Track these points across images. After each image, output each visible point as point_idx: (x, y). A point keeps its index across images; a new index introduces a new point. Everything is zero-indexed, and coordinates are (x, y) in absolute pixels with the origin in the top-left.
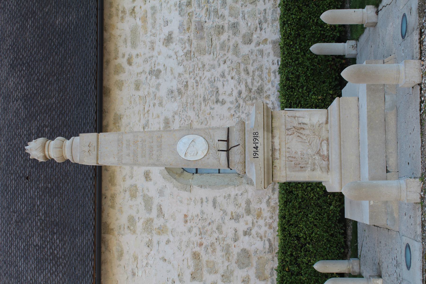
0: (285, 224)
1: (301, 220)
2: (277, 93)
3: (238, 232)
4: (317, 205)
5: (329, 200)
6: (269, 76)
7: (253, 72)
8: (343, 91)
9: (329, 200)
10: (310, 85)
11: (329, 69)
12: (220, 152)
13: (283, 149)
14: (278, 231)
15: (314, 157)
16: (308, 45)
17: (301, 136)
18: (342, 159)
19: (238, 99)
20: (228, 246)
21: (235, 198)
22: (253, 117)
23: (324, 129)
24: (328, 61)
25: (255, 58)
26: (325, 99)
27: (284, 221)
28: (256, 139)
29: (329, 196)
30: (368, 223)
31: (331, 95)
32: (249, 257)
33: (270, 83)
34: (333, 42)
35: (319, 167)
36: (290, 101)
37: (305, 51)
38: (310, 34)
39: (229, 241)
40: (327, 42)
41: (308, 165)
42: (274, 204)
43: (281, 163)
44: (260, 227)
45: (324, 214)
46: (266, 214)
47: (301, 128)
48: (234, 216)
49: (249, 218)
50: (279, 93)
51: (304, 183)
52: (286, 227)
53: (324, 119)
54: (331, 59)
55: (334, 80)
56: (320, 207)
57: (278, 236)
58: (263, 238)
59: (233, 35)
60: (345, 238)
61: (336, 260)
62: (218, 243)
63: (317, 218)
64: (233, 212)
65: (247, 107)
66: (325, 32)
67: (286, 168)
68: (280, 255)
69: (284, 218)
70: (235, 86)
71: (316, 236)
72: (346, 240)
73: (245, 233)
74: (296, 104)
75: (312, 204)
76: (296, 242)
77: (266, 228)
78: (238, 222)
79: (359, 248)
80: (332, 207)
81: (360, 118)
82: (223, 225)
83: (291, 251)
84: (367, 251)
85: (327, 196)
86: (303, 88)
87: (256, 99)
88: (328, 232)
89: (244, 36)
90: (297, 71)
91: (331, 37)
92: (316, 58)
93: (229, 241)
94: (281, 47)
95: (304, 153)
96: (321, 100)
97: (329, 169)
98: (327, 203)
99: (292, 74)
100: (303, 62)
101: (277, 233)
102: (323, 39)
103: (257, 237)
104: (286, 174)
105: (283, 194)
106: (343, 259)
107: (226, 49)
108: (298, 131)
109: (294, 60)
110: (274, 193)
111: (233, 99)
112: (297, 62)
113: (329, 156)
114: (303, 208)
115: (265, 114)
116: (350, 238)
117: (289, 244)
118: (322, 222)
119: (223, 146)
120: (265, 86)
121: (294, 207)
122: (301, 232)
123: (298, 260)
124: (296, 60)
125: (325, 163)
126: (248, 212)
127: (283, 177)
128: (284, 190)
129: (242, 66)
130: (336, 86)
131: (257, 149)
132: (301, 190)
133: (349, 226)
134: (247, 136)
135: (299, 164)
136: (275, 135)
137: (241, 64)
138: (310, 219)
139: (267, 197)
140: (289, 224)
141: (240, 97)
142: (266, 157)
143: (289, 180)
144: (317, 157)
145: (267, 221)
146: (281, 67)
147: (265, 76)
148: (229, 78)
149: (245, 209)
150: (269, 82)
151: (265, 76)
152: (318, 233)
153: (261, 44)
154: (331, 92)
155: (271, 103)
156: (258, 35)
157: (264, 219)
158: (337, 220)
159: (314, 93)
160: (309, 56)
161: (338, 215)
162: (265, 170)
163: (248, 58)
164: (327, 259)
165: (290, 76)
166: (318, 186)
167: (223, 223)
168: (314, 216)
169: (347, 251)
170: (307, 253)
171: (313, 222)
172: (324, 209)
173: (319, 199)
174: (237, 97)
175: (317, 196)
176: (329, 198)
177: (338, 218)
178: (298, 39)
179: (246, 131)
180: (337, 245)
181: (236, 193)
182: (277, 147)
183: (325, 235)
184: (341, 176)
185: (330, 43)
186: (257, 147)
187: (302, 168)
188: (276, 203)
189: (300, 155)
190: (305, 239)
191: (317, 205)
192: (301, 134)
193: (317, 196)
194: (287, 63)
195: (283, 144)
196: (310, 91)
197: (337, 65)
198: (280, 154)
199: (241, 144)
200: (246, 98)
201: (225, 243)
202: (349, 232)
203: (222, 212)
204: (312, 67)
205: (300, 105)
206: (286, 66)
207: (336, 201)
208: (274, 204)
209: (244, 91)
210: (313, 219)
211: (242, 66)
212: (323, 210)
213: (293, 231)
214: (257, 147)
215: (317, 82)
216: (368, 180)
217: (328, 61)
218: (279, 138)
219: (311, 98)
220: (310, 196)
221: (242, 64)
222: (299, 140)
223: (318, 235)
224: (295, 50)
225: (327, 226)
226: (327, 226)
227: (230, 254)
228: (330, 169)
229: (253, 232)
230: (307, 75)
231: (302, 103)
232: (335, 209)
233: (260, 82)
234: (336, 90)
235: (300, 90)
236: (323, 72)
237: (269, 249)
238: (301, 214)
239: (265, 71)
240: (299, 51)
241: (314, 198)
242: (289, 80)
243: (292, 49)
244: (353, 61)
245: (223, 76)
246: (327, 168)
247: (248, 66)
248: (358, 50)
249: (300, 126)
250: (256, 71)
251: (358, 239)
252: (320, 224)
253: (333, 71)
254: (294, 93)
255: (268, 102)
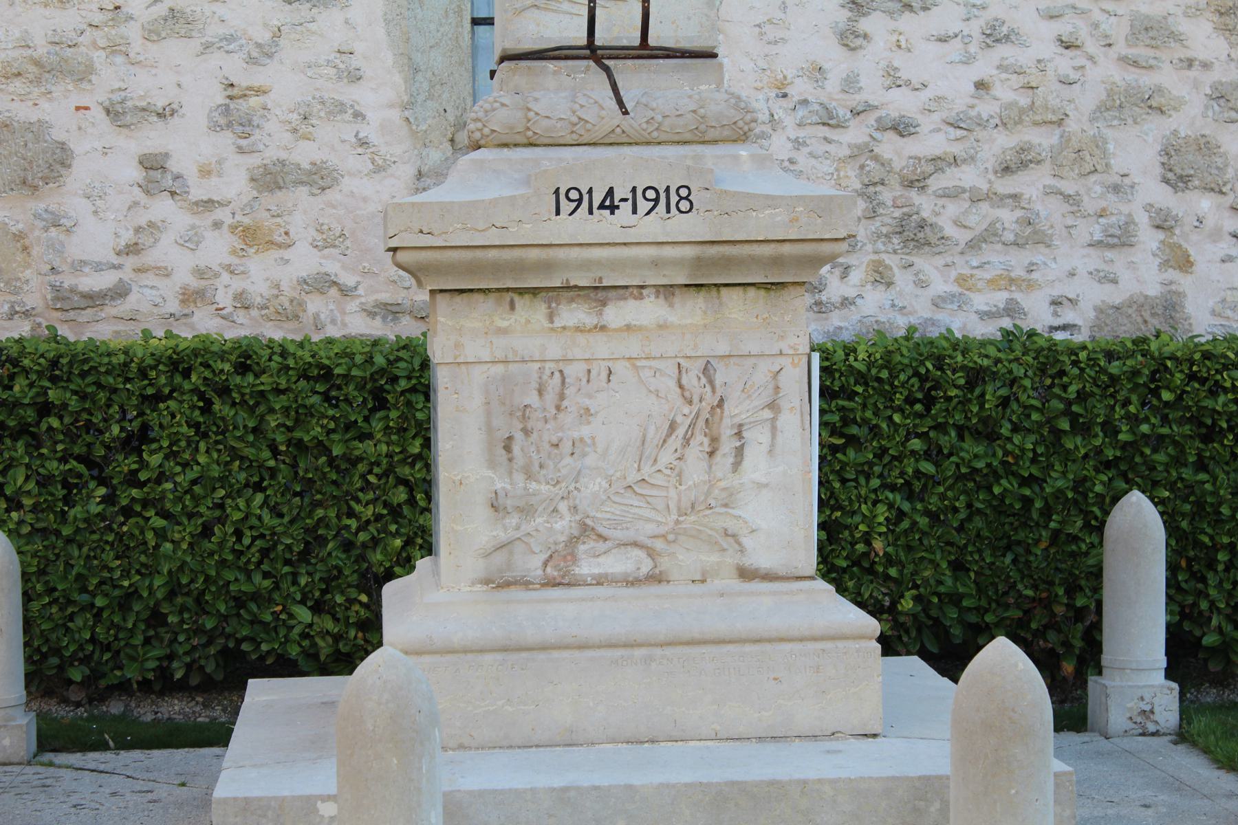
0: (207, 374)
1: (235, 454)
2: (899, 325)
3: (160, 124)
4: (313, 540)
5: (339, 599)
6: (990, 282)
7: (1015, 197)
8: (915, 663)
9: (339, 599)
10: (943, 497)
11: (1029, 593)
12: (585, 12)
13: (601, 347)
14: (169, 335)
15: (563, 507)
16: (1155, 484)
17: (675, 441)
18: (555, 654)
19: (871, 119)
20: (83, 74)
21: (341, 107)
22: (768, 186)
23: (714, 558)
24: (1073, 589)
25: (1090, 205)
26: (871, 571)
27: (227, 367)
28: (657, 200)
29: (364, 598)
30: (220, 792)
31: (894, 604)
32: (27, 185)
33: (956, 289)
34: (1169, 612)
35: (512, 534)
36: (860, 389)
37: (1123, 467)
38: (1215, 493)
39: (109, 77)
40: (1172, 584)
41: (519, 478)
42: (316, 316)
43: (529, 332)
44: (191, 242)
45: (266, 575)
46: (262, 275)
47: (714, 440)
48: (242, 105)
49: (234, 185)
50: (902, 333)
51: (428, 467)
52: (194, 378)
53: (763, 560)
54: (1080, 602)
55: (973, 618)
56: (305, 555)
57: (147, 335)
58: (130, 262)
59: (1214, 87)
60: (145, 686)
61: (26, 644)
62: (98, 18)
63: (247, 541)
64: (268, 100)
65: (827, 167)
66: (1227, 570)
67: (506, 362)
68: (43, 347)
69: (243, 368)
70: (939, 99)
71: (150, 535)
72: (131, 694)
73: (153, 164)
74: (846, 422)
75: (320, 512)
76: (116, 430)
77: (184, 277)
78: (215, 127)
79: (93, 759)
80: (304, 614)
81: (770, 747)
82: (195, 44)
83: (65, 406)
84: (74, 799)
85: (361, 589)
86: (927, 455)
87: (872, 215)
88: (171, 595)
89: (1205, 146)
90: (1016, 429)
91: (1195, 604)
92: (1087, 526)
93: (109, 77)
94: (1145, 340)
95: (584, 455)
96: (865, 555)
97: (499, 586)
98: (324, 592)
99: (1004, 402)
100: (1067, 457)
101: (160, 333)
102: (1189, 560)
103: (138, 230)
104: (474, 365)
105: (369, 360)
106: (29, 678)
107: (1140, 52)
108: (701, 423)
109: (1075, 408)
110: (372, 315)
111: (872, 89)
112: (1065, 425)
113: (569, 585)
114: (294, 466)
115: (786, 249)
116: (146, 712)
117: (102, 396)
118: (223, 562)
119: (618, 26)
120: (939, 261)
121: (301, 416)
122: (171, 455)
123: (20, 445)
124: (1074, 418)
125: (533, 565)
126: (271, 179)
127: (458, 345)
128: (390, 363)
129: (1044, 140)
130: (939, 629)
131: (602, 207)
132: (389, 456)
133: (205, 706)
134: (671, 152)
135: (527, 432)
136: (677, 300)
137: (1058, 132)
138: (241, 503)
139: (348, 280)
140: (210, 394)
141: (882, 127)
142: (561, 254)
143: (442, 379)
144: (564, 525)
145: (225, 277)
146: (1041, 342)
147: (994, 259)
148: (984, 68)
149: (283, 163)
150: (961, 280)
151: (994, 259)
152: (168, 546)
153: (1161, 235)
154: (907, 604)
155: (851, 293)
156: (1210, 222)
157: (236, 261)
158: (239, 642)
159: (901, 514)
160: (1098, 488)
161: (264, 647)
162: (492, 254)
163: (1089, 167)
164: (27, 597)
165: (990, 389)
166: (409, 534)
167: (207, 46)
168: (254, 521)
169: (74, 697)
170: (60, 493)
171: (222, 521)
172: (295, 575)
173: (348, 546)
174: (877, 114)
175: (363, 537)
176: (351, 601)
177: (245, 647)
178: (1187, 429)
179: (699, 149)
180: (108, 647)
181: (369, 115)
182: (617, 313)
183: (158, 582)
184: (466, 651)
185: (1168, 596)
186: (613, 208)
187: (508, 448)
188: (318, 328)
189: (576, 435)
190: (132, 480)
191: (313, 540)
192: (687, 441)
193: (363, 537)
194: (1062, 373)
195: (633, 346)
196: (910, 497)
197: (1052, 636)
198: (578, 329)
199: (625, 122)
200: (876, 158)
201: (99, 57)
202: (175, 708)
203: (264, 36)
204: (1038, 504)
205: (840, 441)
206: (1042, 371)
207: (337, 638)
208: (316, 316)
209: (912, 147)
210: (237, 516)
211: (1044, 140)
212: (287, 569)
213: (175, 417)
214: (613, 208)
215: (961, 529)
216: (446, 788)
217: (1073, 589)
218: (662, 327)
219: (875, 503)
220: (358, 501)
221: (1055, 140)
222: (652, 430)
223: (157, 547)
224: (1128, 417)
225: (203, 593)
226: (203, 593)
227: (37, 81)
228: (504, 594)
229: (162, 208)
230: (998, 478)
231: (851, 453)
232: (297, 630)
233: (963, 237)
234: (919, 630)
235: (916, 444)
236: (1014, 561)
237: (73, 290)
238: (266, 454)
239: (1018, 261)
240: (1121, 437)
241: (353, 523)
242: (971, 385)
243: (1134, 398)
244: (1072, 714)
245: (995, 36)
246: (509, 576)
247: (1047, 167)
248: (1126, 743)
249: (726, 432)
250: (1019, 213)
251: (137, 754)
252: (211, 554)
253: (1019, 614)
254: (901, 410)
255: (856, 276)
